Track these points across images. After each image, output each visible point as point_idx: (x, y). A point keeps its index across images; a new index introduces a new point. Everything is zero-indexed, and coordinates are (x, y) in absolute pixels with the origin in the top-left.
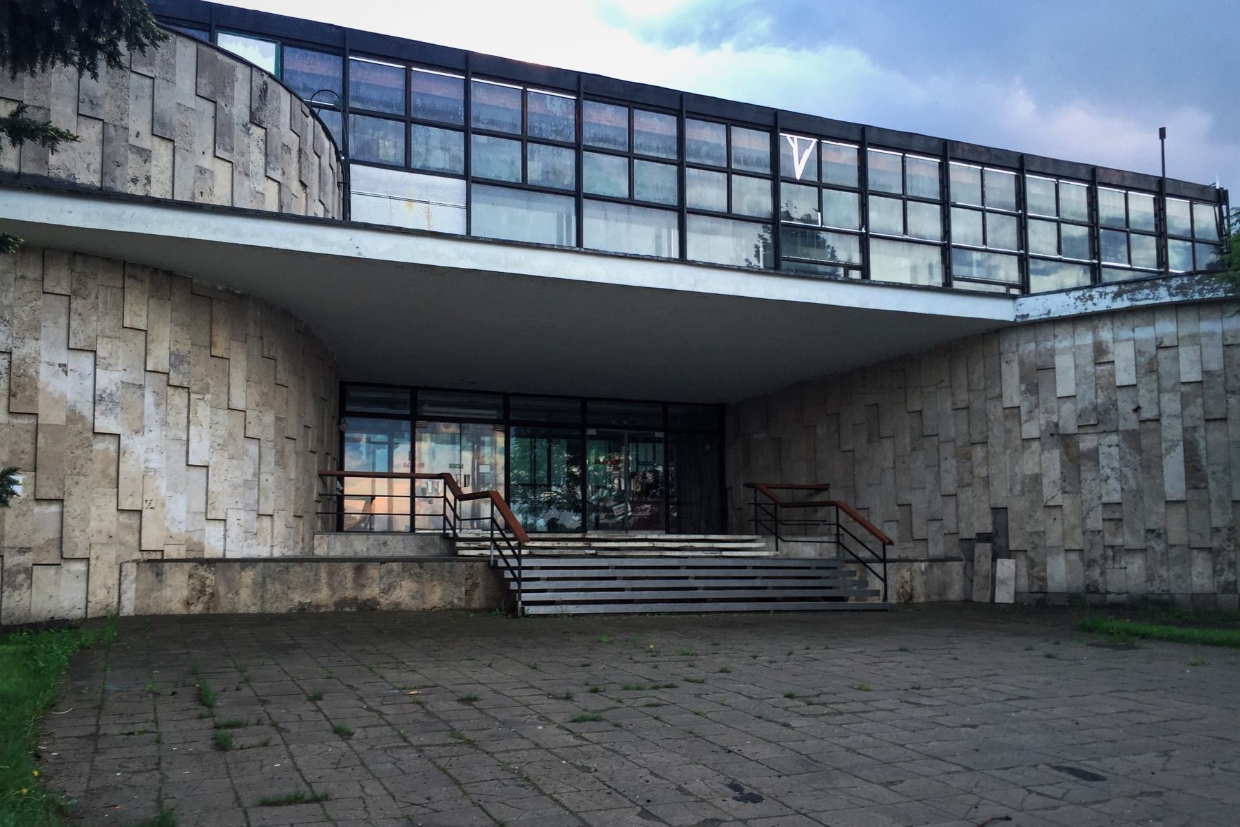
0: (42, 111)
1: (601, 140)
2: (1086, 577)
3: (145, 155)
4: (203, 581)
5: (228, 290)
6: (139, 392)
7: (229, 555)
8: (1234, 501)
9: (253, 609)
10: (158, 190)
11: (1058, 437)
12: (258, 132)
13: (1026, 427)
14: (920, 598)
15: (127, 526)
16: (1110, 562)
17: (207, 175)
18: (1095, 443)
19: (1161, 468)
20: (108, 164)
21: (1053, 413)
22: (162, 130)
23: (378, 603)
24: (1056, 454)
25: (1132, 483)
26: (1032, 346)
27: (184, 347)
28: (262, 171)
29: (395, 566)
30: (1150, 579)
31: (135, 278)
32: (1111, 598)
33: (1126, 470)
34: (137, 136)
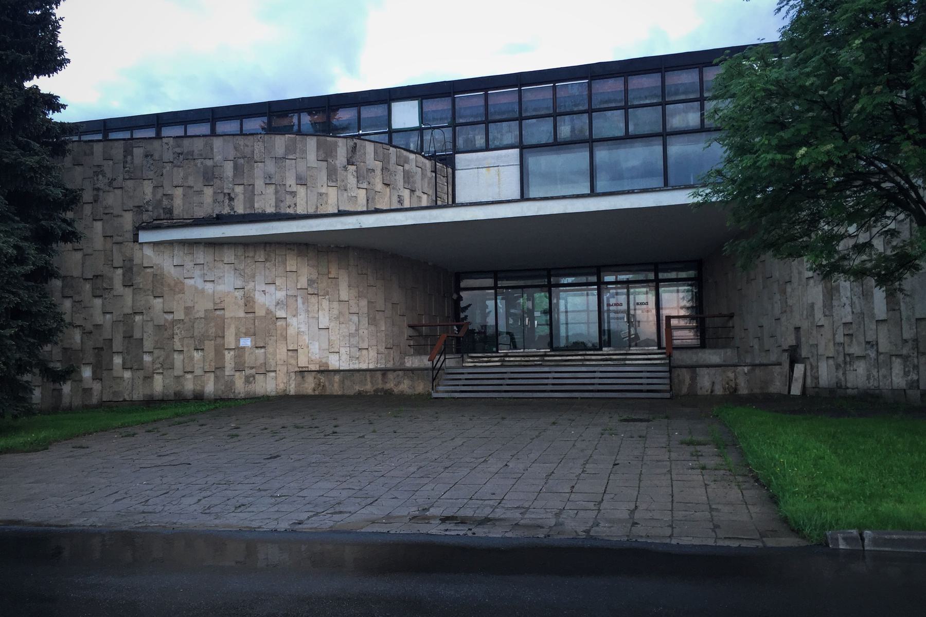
1: (606, 102)
2: (837, 377)
3: (294, 194)
7: (341, 368)
9: (340, 393)
10: (300, 210)
15: (292, 357)
20: (279, 201)
22: (301, 181)
27: (314, 276)
30: (868, 379)
33: (854, 298)
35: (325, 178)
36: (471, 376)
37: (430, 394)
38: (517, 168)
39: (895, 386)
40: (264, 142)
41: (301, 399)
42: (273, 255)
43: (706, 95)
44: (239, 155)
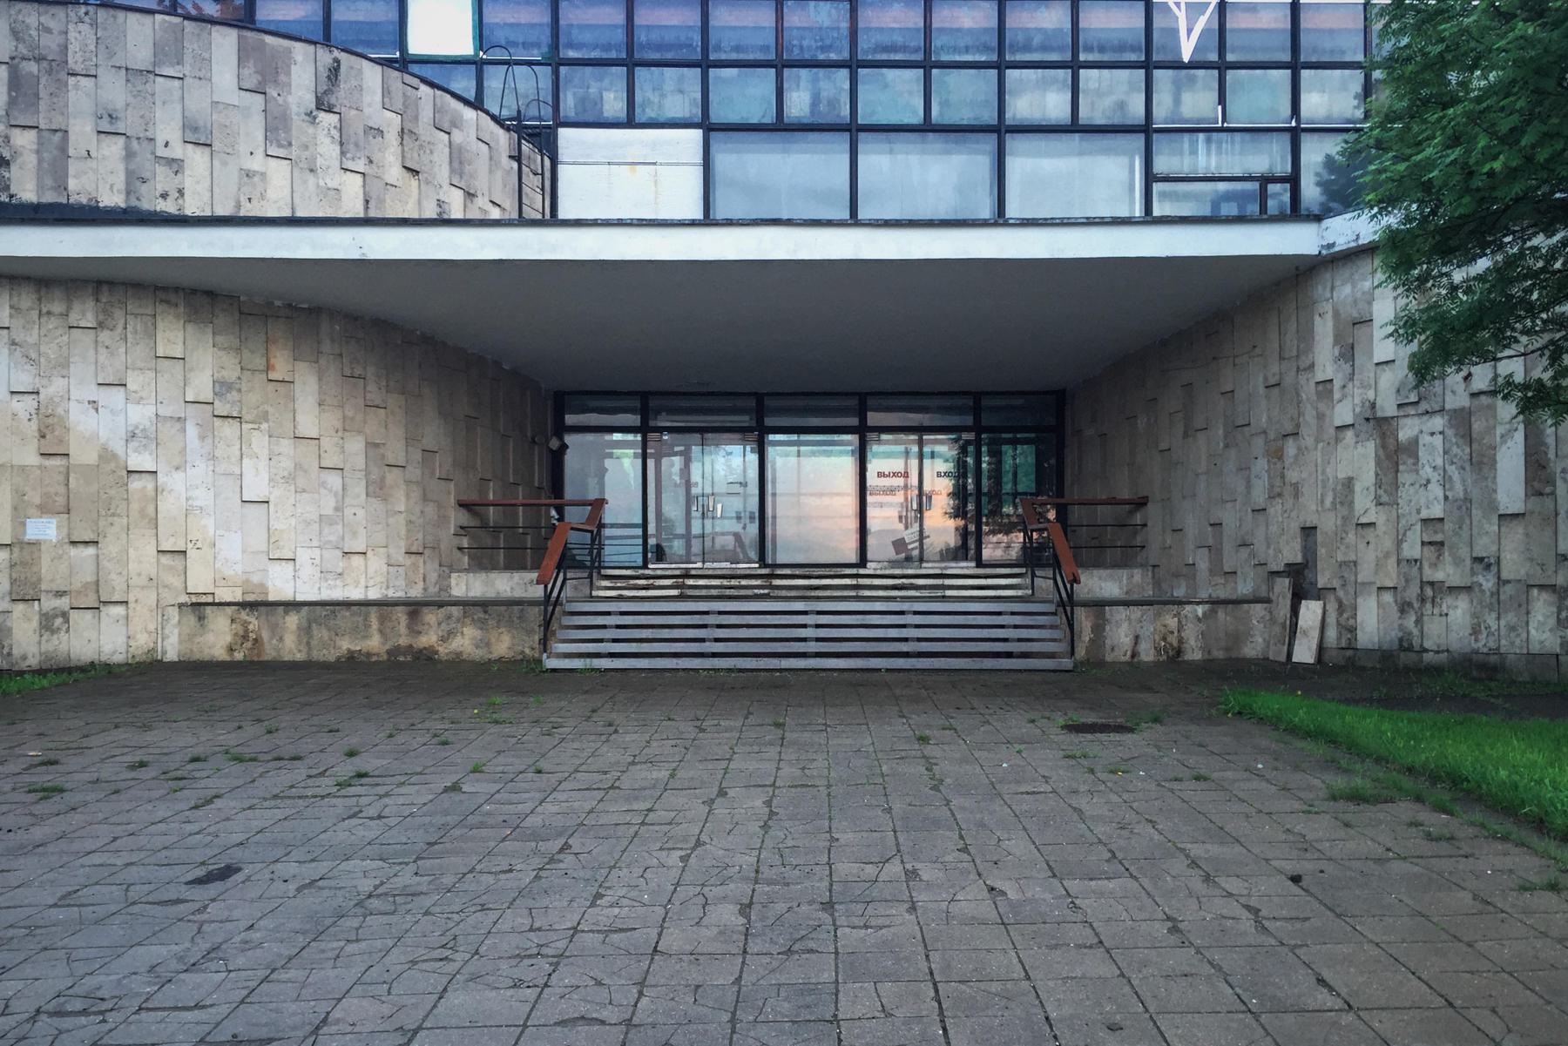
0: (59, 134)
1: (886, 49)
2: (1401, 627)
3: (176, 165)
4: (245, 624)
5: (290, 305)
6: (178, 426)
7: (300, 598)
8: (1501, 516)
9: (299, 657)
10: (192, 208)
11: (1377, 423)
12: (328, 119)
13: (1339, 408)
14: (1194, 654)
15: (171, 568)
16: (1429, 605)
17: (256, 179)
18: (1416, 432)
19: (1494, 462)
20: (134, 179)
21: (1368, 387)
23: (437, 652)
24: (1370, 448)
25: (1459, 487)
26: (1347, 289)
27: (231, 373)
28: (337, 164)
29: (455, 611)
30: (1475, 632)
31: (168, 302)
32: (1428, 657)
33: (1451, 469)
34: (166, 145)
35: (261, 137)
36: (600, 620)
37: (540, 661)
38: (697, 174)
39: (1535, 648)
40: (94, 24)
41: (195, 670)
42: (118, 314)
43: (1082, 57)
44: (23, 50)
